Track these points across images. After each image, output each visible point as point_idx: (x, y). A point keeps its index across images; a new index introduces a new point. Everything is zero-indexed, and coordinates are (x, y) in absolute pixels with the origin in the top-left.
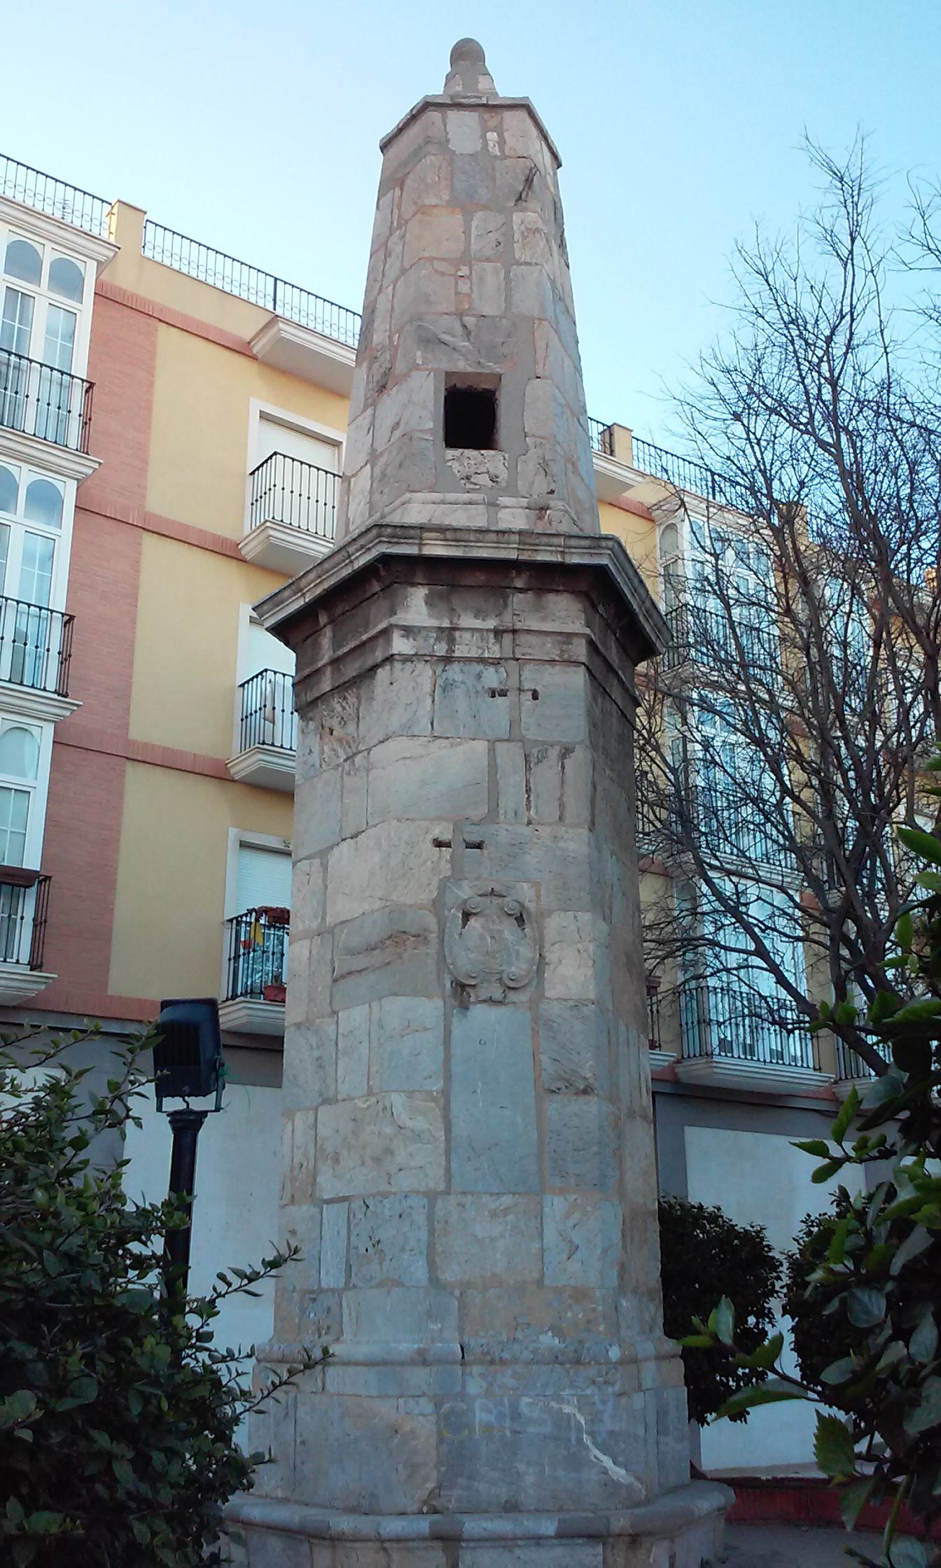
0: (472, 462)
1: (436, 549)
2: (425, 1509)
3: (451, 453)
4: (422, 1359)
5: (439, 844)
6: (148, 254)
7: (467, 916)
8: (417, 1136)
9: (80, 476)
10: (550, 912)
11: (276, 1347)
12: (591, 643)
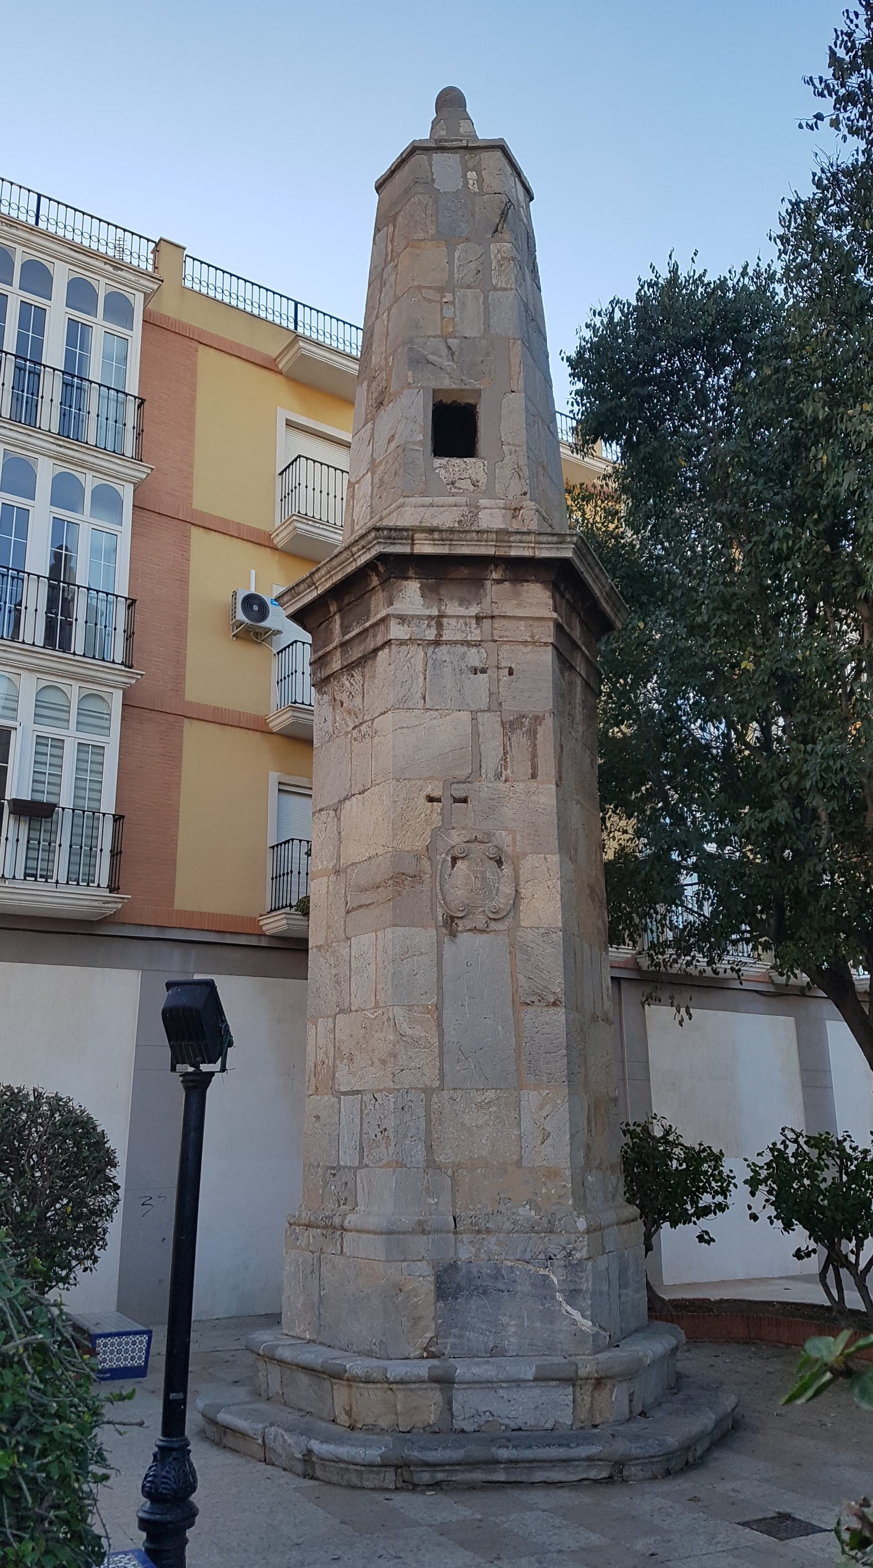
0: (457, 469)
1: (425, 547)
2: (425, 1355)
3: (439, 462)
4: (421, 1229)
5: (431, 799)
6: (188, 284)
7: (454, 860)
8: (415, 1042)
9: (135, 480)
10: (525, 855)
11: (304, 1214)
12: (559, 627)
